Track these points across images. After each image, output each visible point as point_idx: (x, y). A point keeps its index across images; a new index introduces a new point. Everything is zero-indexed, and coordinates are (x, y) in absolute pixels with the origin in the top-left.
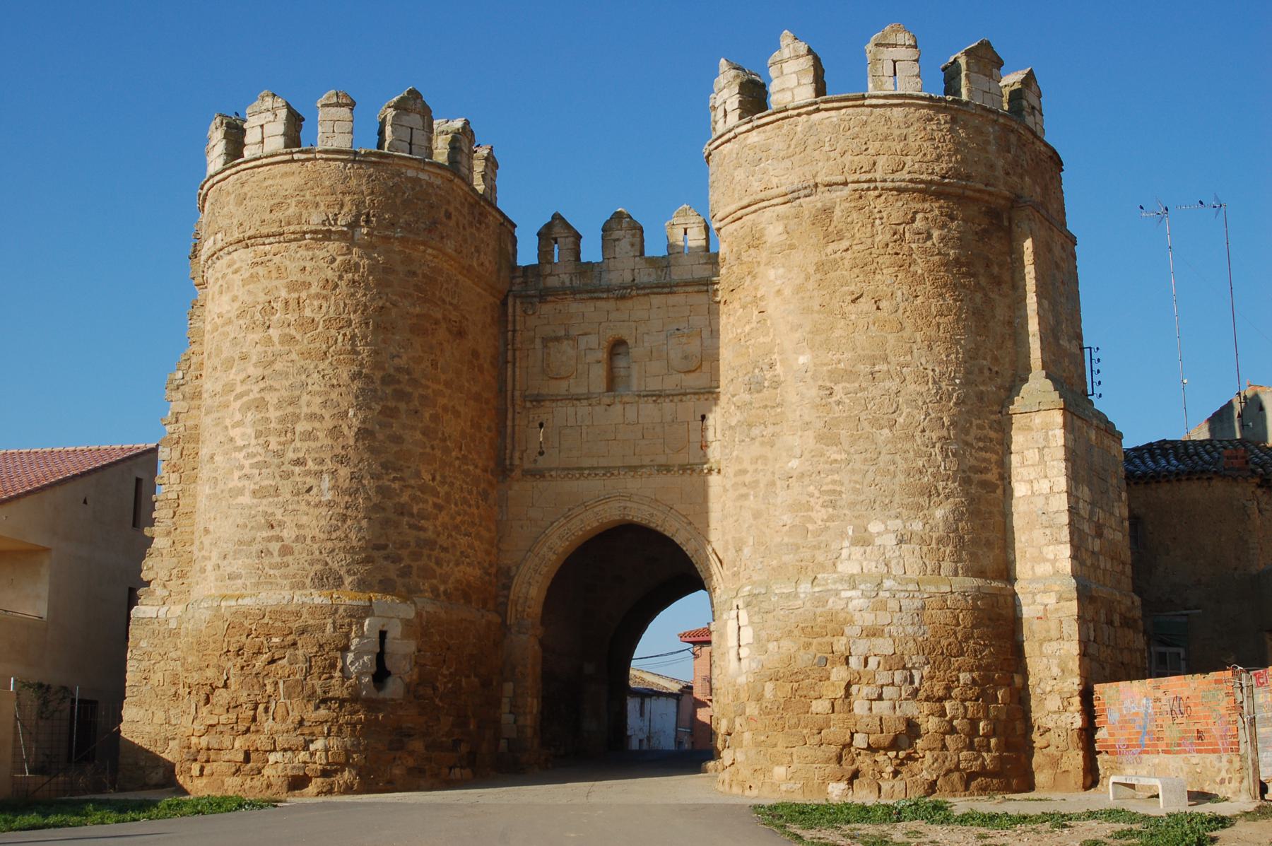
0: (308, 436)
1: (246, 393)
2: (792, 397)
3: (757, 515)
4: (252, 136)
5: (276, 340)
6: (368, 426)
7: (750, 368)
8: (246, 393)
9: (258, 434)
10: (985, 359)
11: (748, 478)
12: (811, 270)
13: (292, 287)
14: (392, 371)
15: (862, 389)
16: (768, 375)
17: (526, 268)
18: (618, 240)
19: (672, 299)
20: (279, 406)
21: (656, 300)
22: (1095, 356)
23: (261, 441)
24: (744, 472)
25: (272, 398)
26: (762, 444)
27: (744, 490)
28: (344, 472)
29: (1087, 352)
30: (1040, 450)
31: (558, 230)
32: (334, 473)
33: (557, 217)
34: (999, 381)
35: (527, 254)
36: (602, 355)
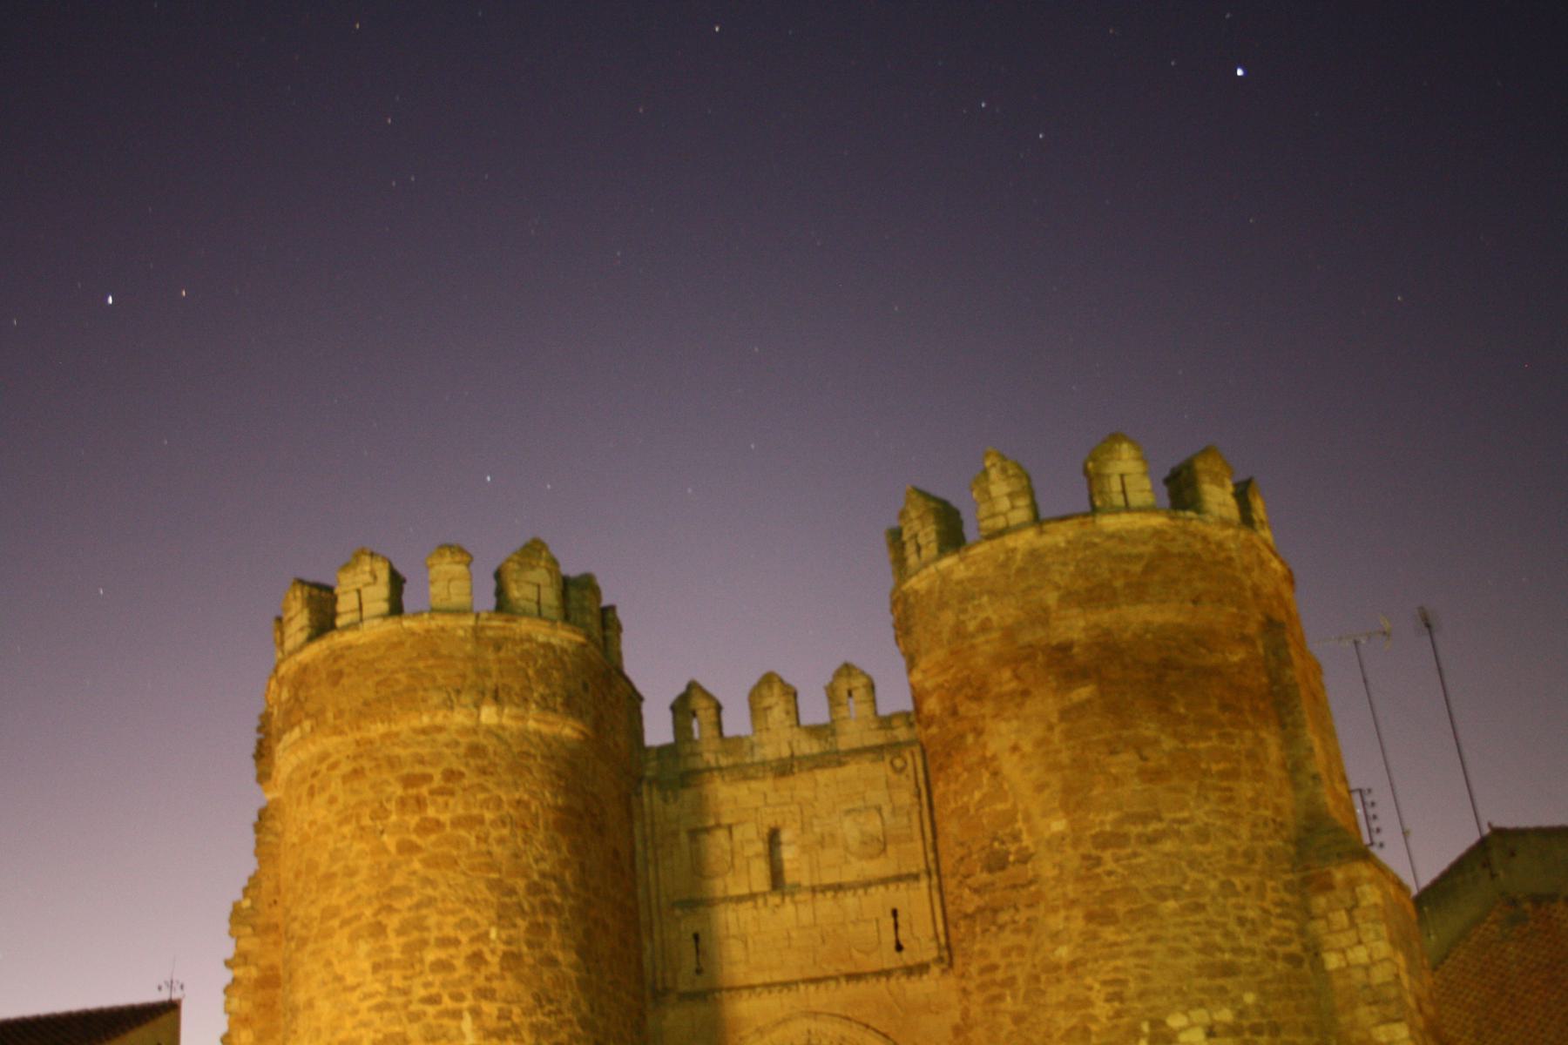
0: (443, 966)
1: (358, 917)
2: (1048, 871)
3: (1018, 1019)
4: (346, 604)
5: (392, 849)
6: (514, 948)
7: (987, 842)
8: (358, 917)
9: (376, 968)
10: (1266, 808)
11: (1000, 975)
12: (1054, 719)
13: (409, 781)
14: (536, 877)
15: (1135, 855)
16: (1013, 848)
17: (661, 750)
18: (770, 708)
19: (842, 773)
20: (401, 932)
21: (823, 776)
22: (1368, 799)
23: (381, 975)
24: (993, 968)
25: (393, 922)
26: (1016, 931)
27: (995, 991)
28: (490, 1008)
29: (1356, 798)
30: (1349, 911)
31: (699, 703)
32: (476, 1013)
33: (692, 686)
34: (1285, 834)
35: (658, 730)
36: (760, 847)
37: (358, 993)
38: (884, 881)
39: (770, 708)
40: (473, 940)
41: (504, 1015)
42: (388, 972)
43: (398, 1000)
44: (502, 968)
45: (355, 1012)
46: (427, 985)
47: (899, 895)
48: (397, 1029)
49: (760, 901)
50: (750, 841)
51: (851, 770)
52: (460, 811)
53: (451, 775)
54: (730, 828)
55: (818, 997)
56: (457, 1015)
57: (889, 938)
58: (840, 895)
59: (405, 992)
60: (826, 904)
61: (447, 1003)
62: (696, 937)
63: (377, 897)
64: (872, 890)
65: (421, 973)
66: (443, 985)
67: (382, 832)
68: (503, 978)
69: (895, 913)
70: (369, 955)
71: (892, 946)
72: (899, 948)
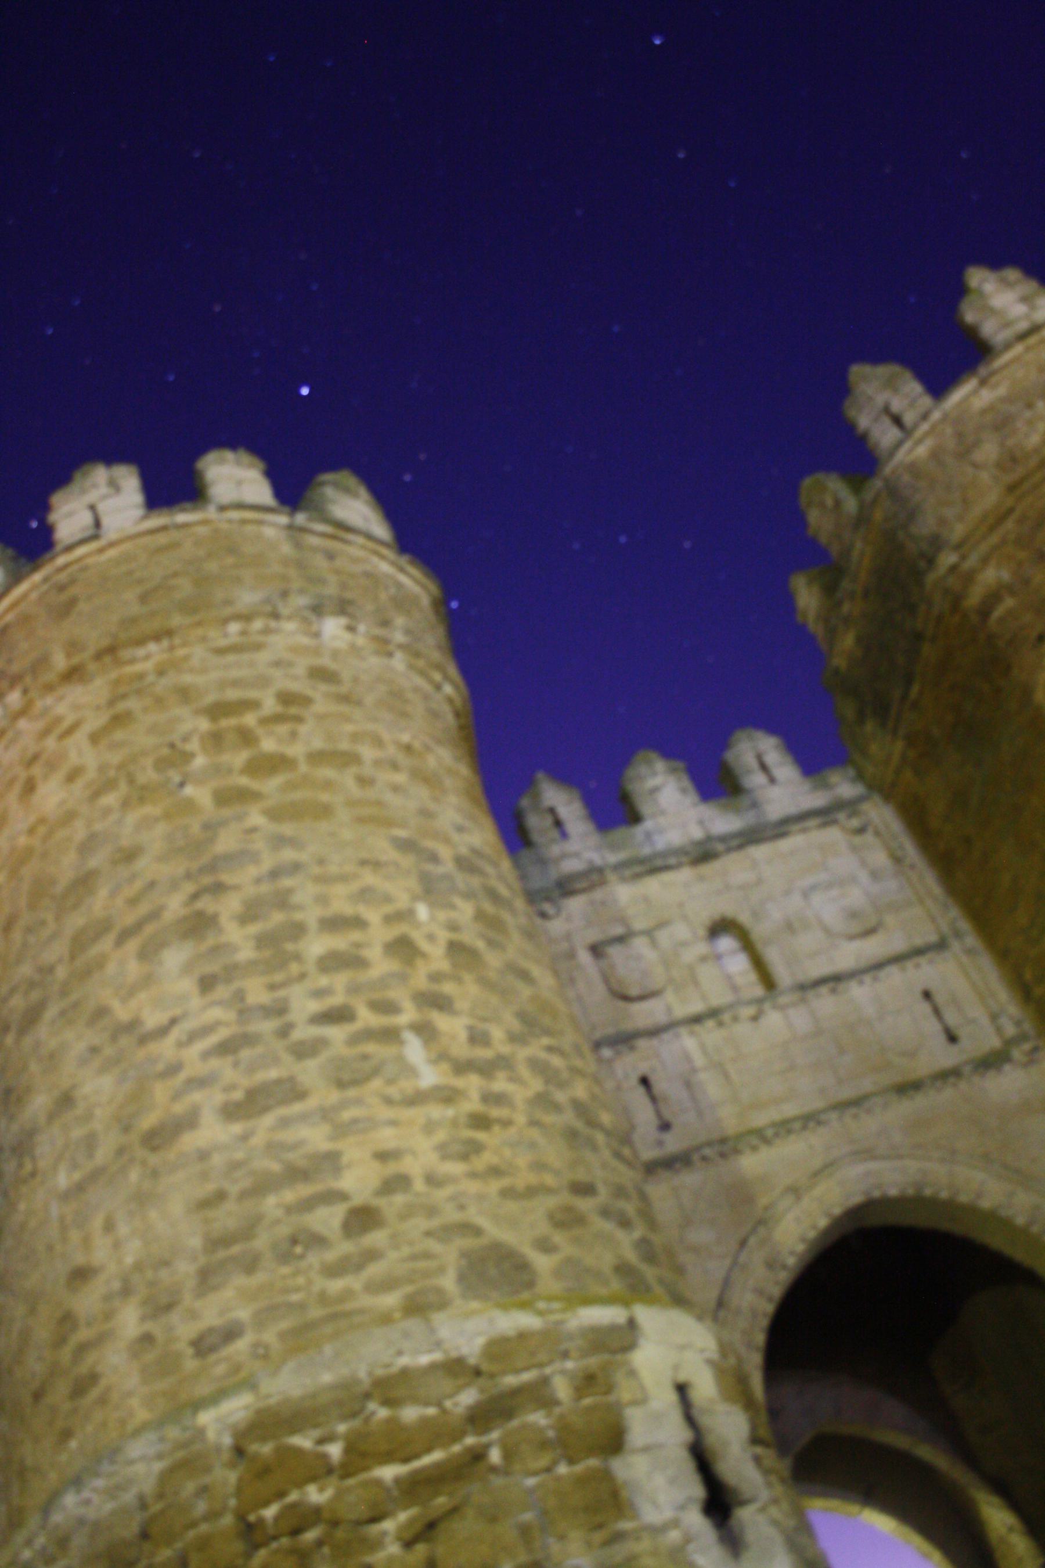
0: (332, 962)
9: (207, 984)
19: (784, 845)
20: (246, 917)
23: (222, 992)
37: (176, 1034)
38: (898, 959)
39: (655, 790)
40: (389, 919)
41: (477, 1038)
42: (236, 985)
43: (267, 1026)
44: (455, 965)
45: (174, 1069)
46: (320, 993)
47: (928, 972)
48: (273, 1074)
49: (726, 1017)
50: (684, 944)
51: (794, 842)
52: (318, 743)
53: (286, 698)
54: (649, 933)
55: (867, 1125)
56: (390, 1035)
57: (932, 1027)
58: (842, 986)
59: (280, 1009)
60: (825, 1003)
61: (366, 1018)
62: (645, 1081)
63: (188, 876)
64: (883, 974)
65: (302, 976)
66: (354, 989)
67: (182, 785)
68: (459, 980)
69: (927, 995)
70: (187, 969)
71: (942, 1038)
72: (952, 1038)
